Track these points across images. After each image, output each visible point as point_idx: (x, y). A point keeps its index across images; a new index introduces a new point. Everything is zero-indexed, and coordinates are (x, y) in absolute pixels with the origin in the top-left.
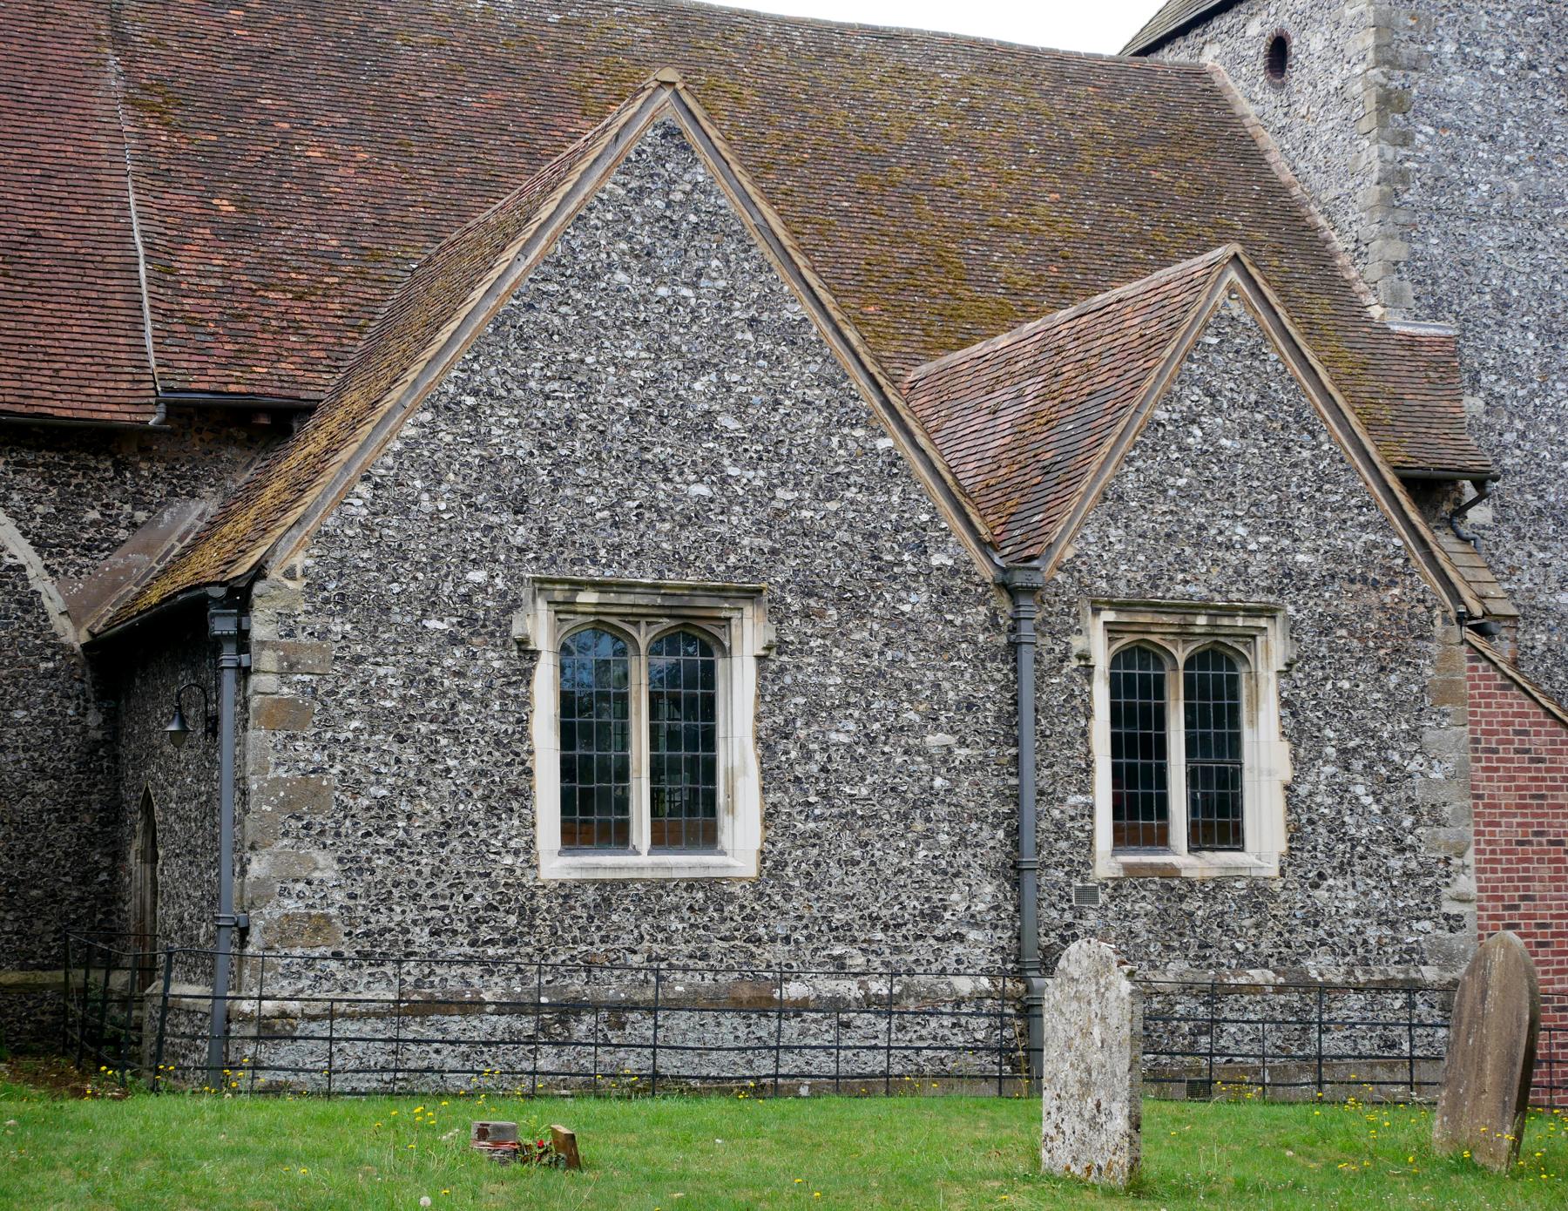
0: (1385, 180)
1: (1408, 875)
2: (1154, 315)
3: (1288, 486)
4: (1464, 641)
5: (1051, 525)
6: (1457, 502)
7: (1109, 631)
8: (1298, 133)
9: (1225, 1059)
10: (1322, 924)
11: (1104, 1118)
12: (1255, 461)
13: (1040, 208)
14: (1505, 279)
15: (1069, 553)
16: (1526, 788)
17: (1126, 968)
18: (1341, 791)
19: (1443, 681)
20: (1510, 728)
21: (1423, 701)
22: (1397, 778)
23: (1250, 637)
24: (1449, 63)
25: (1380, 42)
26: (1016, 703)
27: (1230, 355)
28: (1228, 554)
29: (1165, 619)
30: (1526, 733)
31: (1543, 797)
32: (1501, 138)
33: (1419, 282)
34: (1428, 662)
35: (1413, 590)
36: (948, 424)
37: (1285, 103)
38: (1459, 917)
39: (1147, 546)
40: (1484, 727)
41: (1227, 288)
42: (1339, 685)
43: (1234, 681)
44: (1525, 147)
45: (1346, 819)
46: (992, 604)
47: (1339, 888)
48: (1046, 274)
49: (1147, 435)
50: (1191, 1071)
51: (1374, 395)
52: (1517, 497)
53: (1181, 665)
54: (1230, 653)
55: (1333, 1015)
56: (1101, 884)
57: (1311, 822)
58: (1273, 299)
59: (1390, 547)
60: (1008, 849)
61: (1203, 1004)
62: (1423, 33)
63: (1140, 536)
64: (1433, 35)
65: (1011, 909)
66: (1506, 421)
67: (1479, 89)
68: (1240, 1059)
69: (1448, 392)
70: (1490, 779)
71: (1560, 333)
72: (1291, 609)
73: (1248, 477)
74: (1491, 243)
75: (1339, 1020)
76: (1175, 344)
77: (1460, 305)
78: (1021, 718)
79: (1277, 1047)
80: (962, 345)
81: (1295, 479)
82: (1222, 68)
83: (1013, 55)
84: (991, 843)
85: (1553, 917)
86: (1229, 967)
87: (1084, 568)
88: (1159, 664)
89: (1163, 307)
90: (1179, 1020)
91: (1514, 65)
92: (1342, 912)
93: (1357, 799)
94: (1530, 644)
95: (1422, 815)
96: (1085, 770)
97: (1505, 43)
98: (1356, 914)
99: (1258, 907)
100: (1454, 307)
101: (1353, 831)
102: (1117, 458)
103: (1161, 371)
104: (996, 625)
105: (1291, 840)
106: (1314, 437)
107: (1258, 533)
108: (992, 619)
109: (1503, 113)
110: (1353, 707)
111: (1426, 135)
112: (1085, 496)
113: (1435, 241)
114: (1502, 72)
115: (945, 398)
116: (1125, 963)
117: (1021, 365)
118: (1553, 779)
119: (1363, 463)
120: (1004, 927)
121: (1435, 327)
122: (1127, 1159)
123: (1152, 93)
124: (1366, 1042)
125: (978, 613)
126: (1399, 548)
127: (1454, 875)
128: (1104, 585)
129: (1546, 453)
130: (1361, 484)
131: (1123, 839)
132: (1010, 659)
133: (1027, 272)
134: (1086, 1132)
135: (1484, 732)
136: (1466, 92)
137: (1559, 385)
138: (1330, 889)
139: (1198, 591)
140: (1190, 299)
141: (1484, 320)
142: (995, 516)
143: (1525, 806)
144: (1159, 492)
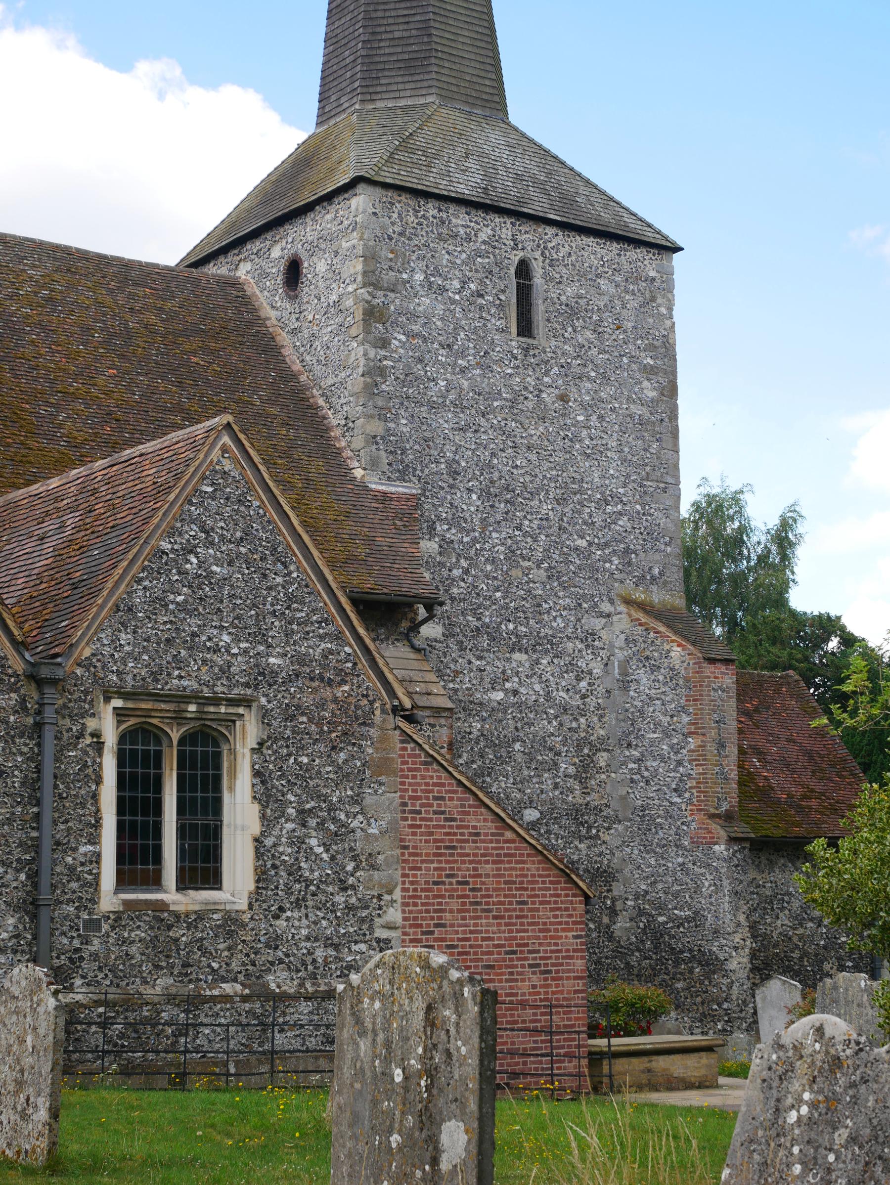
0: (368, 373)
1: (349, 908)
2: (165, 467)
3: (264, 604)
4: (397, 727)
5: (73, 630)
6: (413, 620)
7: (118, 715)
8: (306, 333)
9: (199, 1055)
10: (281, 947)
11: (31, 1110)
12: (239, 584)
13: (100, 380)
14: (456, 453)
15: (87, 653)
16: (442, 841)
17: (53, 987)
18: (298, 842)
19: (380, 758)
20: (431, 795)
21: (364, 773)
22: (343, 833)
23: (230, 721)
24: (418, 288)
25: (367, 268)
26: (39, 772)
27: (222, 501)
28: (215, 656)
29: (163, 706)
30: (443, 798)
31: (454, 848)
32: (456, 347)
33: (391, 452)
34: (369, 743)
35: (359, 687)
36: (8, 547)
37: (297, 311)
38: (387, 941)
39: (151, 648)
40: (410, 793)
41: (221, 448)
42: (300, 760)
43: (218, 756)
44: (474, 356)
45: (302, 864)
46: (22, 691)
47: (295, 919)
48: (101, 432)
49: (153, 560)
50: (172, 1065)
51: (353, 537)
52: (461, 618)
53: (175, 743)
54: (215, 734)
55: (287, 1018)
56: (104, 916)
57: (274, 866)
58: (257, 459)
59: (343, 654)
60: (29, 888)
61: (183, 1011)
62: (399, 264)
63: (145, 640)
64: (407, 266)
65: (29, 937)
66: (454, 560)
67: (440, 309)
68: (212, 1055)
69: (409, 537)
70: (414, 834)
71: (496, 496)
72: (263, 700)
73: (232, 596)
74: (446, 426)
75: (292, 1023)
76: (178, 490)
77: (422, 471)
78: (43, 783)
79: (242, 1045)
80: (28, 483)
81: (269, 599)
82: (252, 281)
83: (87, 260)
84: (15, 884)
85: (459, 940)
86: (206, 982)
87: (99, 664)
88: (158, 742)
89: (172, 461)
90: (164, 1025)
91: (467, 293)
92: (297, 937)
93: (311, 849)
94: (468, 730)
95: (361, 861)
96: (94, 825)
97: (461, 276)
98: (308, 938)
99: (231, 934)
100: (417, 472)
101: (307, 874)
102: (129, 578)
103: (166, 511)
104: (25, 709)
105: (258, 881)
106: (286, 567)
107: (240, 641)
108: (21, 703)
109: (457, 328)
110: (310, 778)
111: (400, 341)
112: (102, 607)
113: (404, 421)
114: (457, 297)
115: (7, 526)
116: (52, 984)
117: (65, 502)
118: (462, 834)
119: (324, 588)
120: (23, 952)
121: (403, 487)
122: (46, 1143)
123: (197, 296)
124: (312, 1039)
125: (10, 699)
126: (349, 654)
127: (385, 908)
128: (114, 678)
129: (483, 585)
130: (321, 604)
131: (123, 880)
132: (35, 736)
133: (86, 430)
134: (18, 1122)
135: (410, 798)
136: (430, 311)
137: (494, 535)
138: (288, 919)
139: (190, 684)
140: (191, 456)
141: (440, 483)
142: (34, 622)
143: (441, 855)
144: (162, 606)
